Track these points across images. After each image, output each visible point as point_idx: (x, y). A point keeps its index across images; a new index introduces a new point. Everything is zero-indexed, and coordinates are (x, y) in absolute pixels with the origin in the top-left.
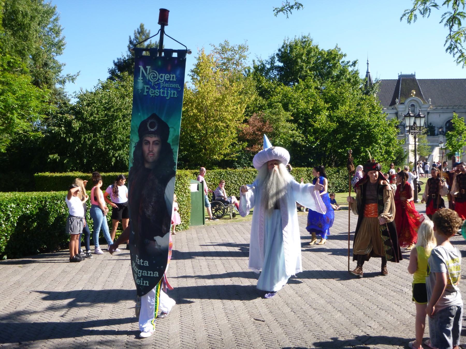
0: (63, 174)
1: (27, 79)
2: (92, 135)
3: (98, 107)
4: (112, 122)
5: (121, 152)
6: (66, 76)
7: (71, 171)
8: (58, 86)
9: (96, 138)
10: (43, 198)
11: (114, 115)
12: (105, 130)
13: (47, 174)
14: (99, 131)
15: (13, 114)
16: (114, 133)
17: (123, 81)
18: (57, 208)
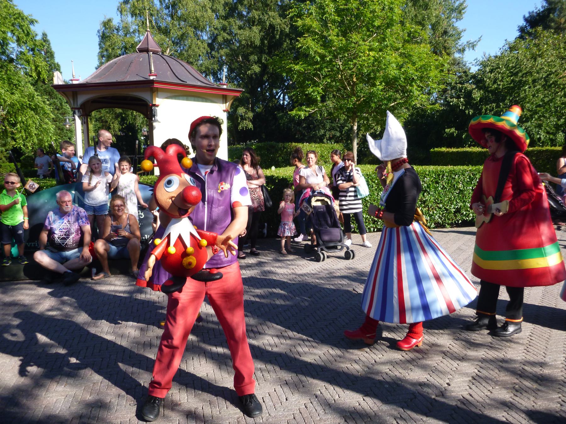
0: (460, 150)
1: (425, 48)
2: (494, 105)
3: (503, 73)
4: (519, 89)
5: (529, 124)
6: (465, 43)
7: (469, 146)
8: (457, 55)
9: (499, 109)
10: (441, 171)
11: (521, 80)
12: (509, 99)
13: (444, 149)
14: (503, 101)
15: (412, 86)
16: (521, 101)
17: (535, 39)
18: (455, 183)
